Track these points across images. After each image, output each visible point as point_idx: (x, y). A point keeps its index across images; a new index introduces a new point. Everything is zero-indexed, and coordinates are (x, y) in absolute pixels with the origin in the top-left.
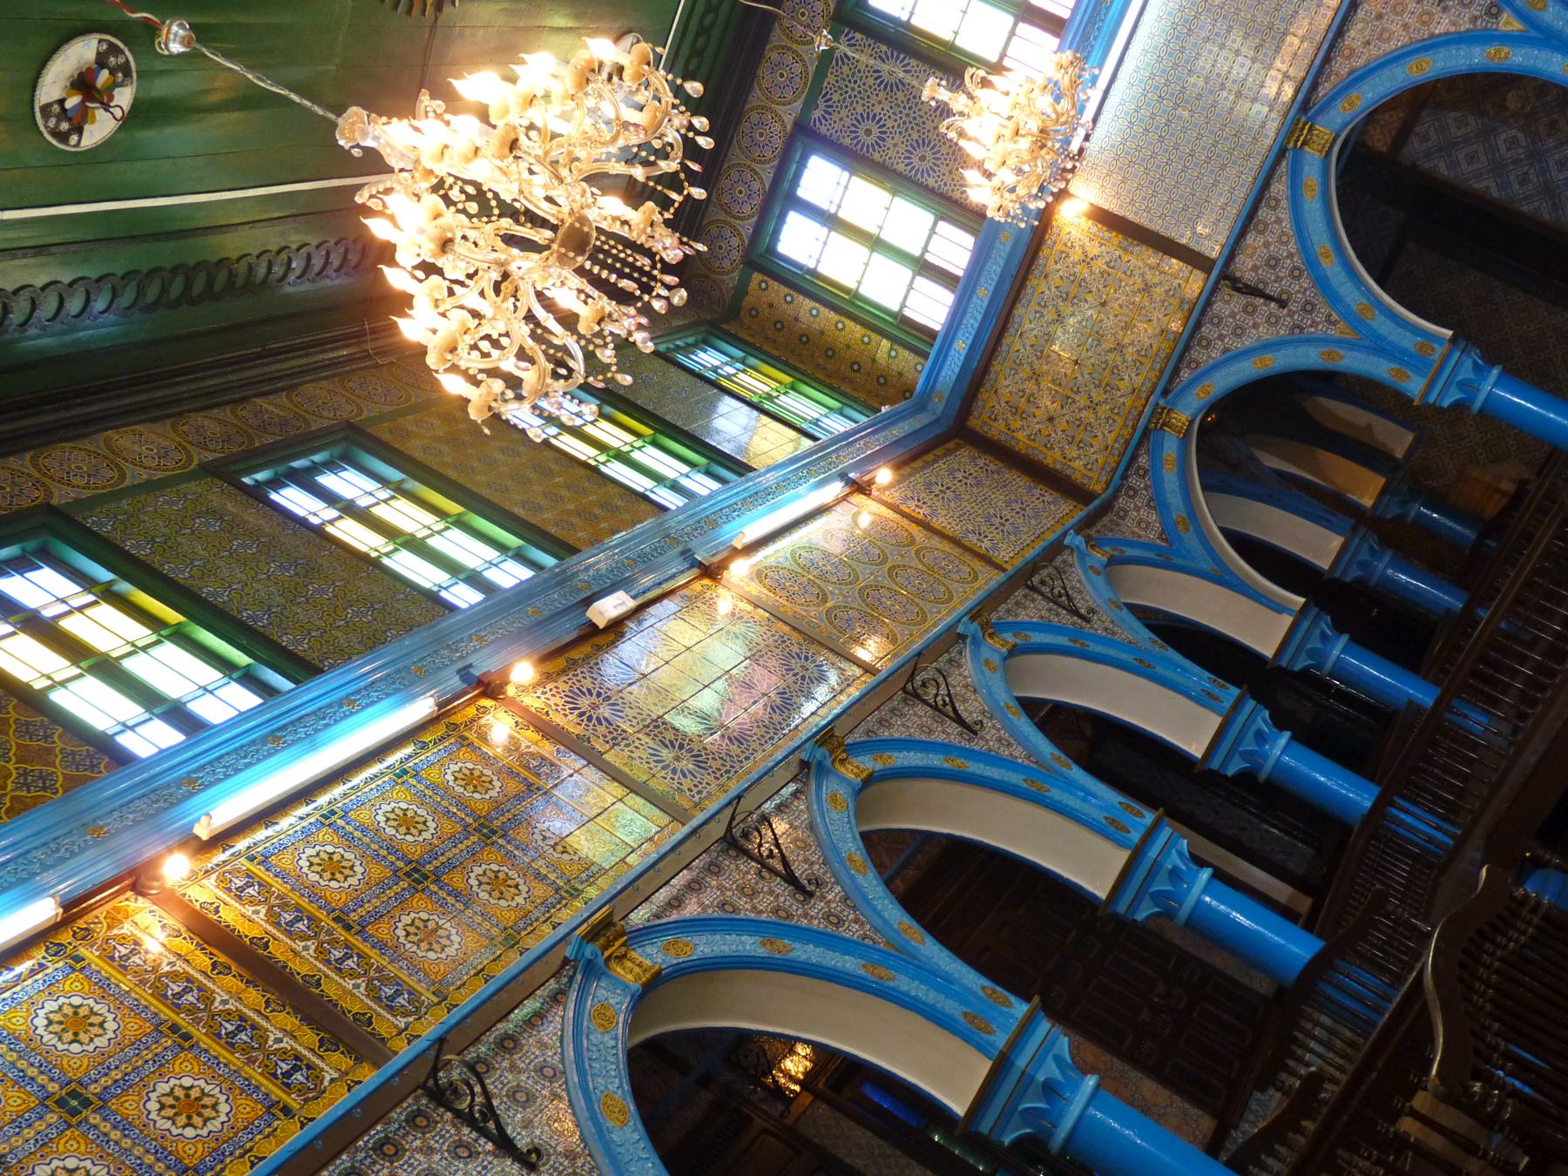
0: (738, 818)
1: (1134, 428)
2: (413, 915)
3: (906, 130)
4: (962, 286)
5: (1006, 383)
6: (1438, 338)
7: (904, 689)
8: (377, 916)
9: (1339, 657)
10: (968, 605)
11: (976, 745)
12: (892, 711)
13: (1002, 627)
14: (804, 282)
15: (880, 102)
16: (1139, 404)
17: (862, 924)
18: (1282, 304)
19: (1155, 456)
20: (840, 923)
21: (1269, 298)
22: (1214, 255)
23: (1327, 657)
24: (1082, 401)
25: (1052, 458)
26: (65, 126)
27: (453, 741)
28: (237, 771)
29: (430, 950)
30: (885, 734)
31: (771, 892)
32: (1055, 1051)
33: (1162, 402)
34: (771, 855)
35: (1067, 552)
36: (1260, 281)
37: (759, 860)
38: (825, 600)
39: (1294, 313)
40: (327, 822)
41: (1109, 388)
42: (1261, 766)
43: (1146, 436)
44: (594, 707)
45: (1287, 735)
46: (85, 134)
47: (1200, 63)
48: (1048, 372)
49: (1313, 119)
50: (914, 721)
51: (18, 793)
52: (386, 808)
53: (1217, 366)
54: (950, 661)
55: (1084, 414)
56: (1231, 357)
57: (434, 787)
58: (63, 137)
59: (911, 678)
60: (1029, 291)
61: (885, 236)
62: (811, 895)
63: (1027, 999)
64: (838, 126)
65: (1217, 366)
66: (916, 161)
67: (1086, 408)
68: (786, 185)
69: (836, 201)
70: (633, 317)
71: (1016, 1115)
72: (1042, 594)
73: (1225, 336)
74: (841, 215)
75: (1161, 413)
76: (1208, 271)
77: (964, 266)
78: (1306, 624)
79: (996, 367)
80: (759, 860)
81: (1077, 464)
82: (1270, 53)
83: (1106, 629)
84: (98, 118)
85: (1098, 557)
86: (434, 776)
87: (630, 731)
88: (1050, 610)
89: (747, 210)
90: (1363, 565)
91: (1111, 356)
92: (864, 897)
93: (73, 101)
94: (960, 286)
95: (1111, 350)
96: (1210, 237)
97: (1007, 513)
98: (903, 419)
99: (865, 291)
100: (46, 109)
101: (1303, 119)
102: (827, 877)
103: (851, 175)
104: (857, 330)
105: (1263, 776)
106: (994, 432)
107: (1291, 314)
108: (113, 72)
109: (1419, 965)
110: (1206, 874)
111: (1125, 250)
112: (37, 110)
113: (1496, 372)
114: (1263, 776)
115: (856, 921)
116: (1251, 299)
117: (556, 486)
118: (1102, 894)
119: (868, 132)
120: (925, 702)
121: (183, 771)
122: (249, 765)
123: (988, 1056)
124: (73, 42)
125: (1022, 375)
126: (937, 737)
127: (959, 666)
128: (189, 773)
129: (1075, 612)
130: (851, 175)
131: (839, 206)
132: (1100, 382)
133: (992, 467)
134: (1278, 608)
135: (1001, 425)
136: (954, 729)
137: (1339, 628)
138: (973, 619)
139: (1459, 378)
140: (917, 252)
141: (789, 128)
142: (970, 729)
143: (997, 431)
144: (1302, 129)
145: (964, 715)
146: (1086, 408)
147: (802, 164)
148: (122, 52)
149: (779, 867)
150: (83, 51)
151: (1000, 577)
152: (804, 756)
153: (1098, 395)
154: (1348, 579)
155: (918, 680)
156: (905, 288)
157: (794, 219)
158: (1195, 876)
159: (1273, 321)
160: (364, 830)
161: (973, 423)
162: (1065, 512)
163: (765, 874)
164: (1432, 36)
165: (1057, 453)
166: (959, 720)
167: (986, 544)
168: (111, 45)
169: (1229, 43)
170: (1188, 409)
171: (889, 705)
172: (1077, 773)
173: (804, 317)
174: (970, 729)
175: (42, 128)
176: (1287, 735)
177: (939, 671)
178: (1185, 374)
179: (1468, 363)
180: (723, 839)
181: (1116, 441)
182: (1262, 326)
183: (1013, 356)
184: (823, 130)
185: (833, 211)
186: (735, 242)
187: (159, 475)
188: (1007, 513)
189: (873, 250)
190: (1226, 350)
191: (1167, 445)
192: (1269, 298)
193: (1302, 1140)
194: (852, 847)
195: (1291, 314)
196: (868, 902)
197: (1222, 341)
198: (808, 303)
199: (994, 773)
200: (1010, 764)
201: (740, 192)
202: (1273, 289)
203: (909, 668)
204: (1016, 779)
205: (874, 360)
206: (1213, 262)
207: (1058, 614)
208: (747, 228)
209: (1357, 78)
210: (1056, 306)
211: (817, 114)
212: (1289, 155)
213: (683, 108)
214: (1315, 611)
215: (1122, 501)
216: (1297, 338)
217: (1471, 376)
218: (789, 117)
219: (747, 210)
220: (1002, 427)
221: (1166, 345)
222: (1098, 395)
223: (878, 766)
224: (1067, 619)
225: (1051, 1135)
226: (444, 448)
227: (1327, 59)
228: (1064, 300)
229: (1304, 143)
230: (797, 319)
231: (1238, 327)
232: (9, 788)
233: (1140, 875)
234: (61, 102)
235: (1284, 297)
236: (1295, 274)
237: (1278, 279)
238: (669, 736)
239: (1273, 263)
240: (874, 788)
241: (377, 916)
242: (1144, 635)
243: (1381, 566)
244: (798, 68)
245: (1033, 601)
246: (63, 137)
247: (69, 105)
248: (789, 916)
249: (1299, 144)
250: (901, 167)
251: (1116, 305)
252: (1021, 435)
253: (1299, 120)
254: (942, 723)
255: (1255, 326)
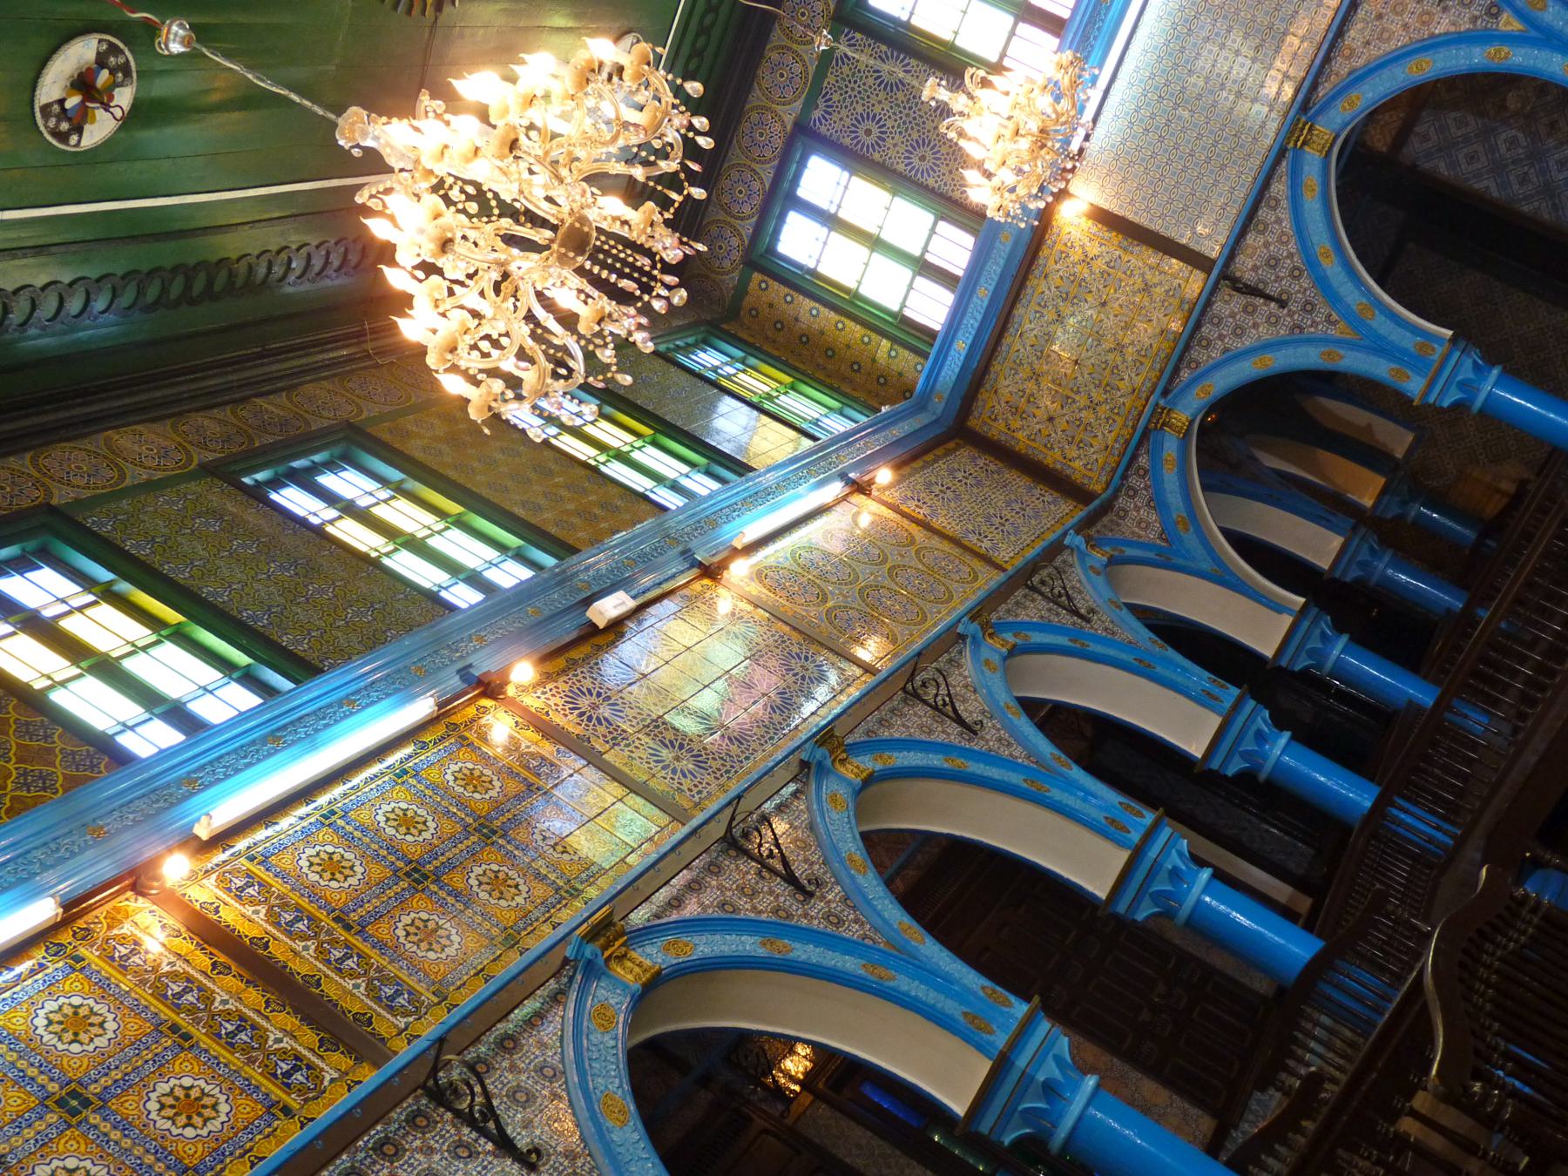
0: (738, 818)
1: (1134, 428)
2: (413, 915)
3: (906, 130)
4: (962, 286)
5: (1006, 383)
6: (1438, 338)
7: (904, 689)
8: (377, 916)
9: (1339, 657)
10: (968, 605)
11: (976, 745)
12: (892, 711)
13: (1002, 627)
14: (804, 282)
15: (880, 102)
16: (1139, 404)
17: (862, 924)
18: (1282, 304)
19: (1155, 456)
20: (840, 923)
21: (1269, 298)
22: (1214, 255)
23: (1327, 657)
24: (1082, 401)
25: (1052, 458)
26: (65, 126)
27: (453, 741)
28: (237, 771)
29: (430, 950)
30: (885, 734)
31: (771, 892)
32: (1055, 1051)
33: (1162, 402)
34: (771, 855)
35: (1067, 552)
36: (1260, 281)
37: (759, 860)
38: (825, 600)
39: (1294, 313)
40: (327, 822)
41: (1109, 388)
42: (1261, 766)
43: (1146, 436)
44: (594, 707)
45: (1287, 735)
46: (85, 134)
47: (1200, 63)
48: (1048, 372)
49: (1313, 119)
50: (914, 721)
51: (18, 793)
52: (386, 808)
53: (1217, 366)
54: (950, 661)
55: (1084, 414)
56: (1231, 357)
57: (434, 787)
58: (63, 137)
59: (911, 678)
60: (1029, 291)
61: (885, 236)
62: (811, 895)
63: (1027, 999)
64: (838, 126)
65: (1217, 366)
66: (916, 161)
67: (1086, 408)
68: (786, 185)
69: (836, 201)
70: (633, 317)
71: (1016, 1115)
72: (1042, 594)
73: (1225, 336)
74: (841, 215)
75: (1161, 413)
76: (1208, 271)
77: (964, 266)
78: (1306, 624)
79: (996, 367)
80: (759, 860)
81: (1077, 464)
82: (1270, 53)
83: (1106, 629)
84: (98, 118)
85: (1098, 557)
86: (434, 776)
87: (630, 731)
88: (1050, 610)
89: (747, 210)
90: (1363, 565)
91: (1111, 356)
92: (864, 897)
93: (73, 101)
94: (960, 286)
95: (1111, 350)
96: (1210, 237)
97: (1007, 513)
98: (903, 419)
99: (865, 291)
100: (46, 109)
101: (1303, 119)
102: (827, 877)
103: (851, 175)
104: (857, 330)
105: (1263, 776)
106: (994, 432)
107: (1291, 314)
108: (113, 72)
109: (1419, 965)
110: (1206, 874)
111: (1125, 250)
112: (37, 110)
113: (1496, 372)
114: (1263, 776)
115: (856, 921)
116: (1251, 299)
117: (556, 486)
118: (1102, 894)
119: (868, 132)
120: (925, 702)
121: (183, 771)
122: (249, 765)
123: (988, 1056)
124: (73, 42)
125: (1022, 375)
126: (937, 737)
127: (959, 666)
128: (189, 773)
129: (1075, 612)
130: (851, 175)
131: (839, 206)
132: (1100, 382)
133: (992, 467)
134: (1278, 608)
135: (1001, 425)
136: (954, 729)
137: (1339, 628)
138: (973, 619)
139: (1459, 378)
140: (917, 252)
141: (789, 128)
142: (970, 729)
143: (997, 431)
144: (1302, 129)
145: (964, 715)
146: (1086, 408)
147: (802, 164)
148: (122, 52)
149: (779, 867)
150: (83, 51)
151: (1000, 577)
152: (804, 756)
153: (1098, 395)
154: (1348, 579)
155: (918, 680)
156: (905, 288)
157: (794, 219)
158: (1195, 876)
159: (1273, 321)
160: (364, 830)
161: (973, 423)
162: (1065, 512)
163: (765, 874)
164: (1432, 36)
165: (1057, 453)
166: (959, 720)
167: (986, 544)
168: (111, 45)
169: (1229, 43)
170: (1188, 409)
171: (889, 705)
172: (1077, 773)
173: (804, 317)
174: (970, 729)
175: (42, 128)
176: (1287, 735)
177: (939, 671)
178: (1185, 374)
179: (1468, 363)
180: (723, 839)
181: (1116, 441)
182: (1262, 326)
183: (1013, 356)
184: (823, 130)
185: (833, 211)
186: (735, 242)
187: (159, 475)
188: (1007, 513)
189: (873, 250)
190: (1226, 350)
191: (1167, 445)
192: (1269, 298)
193: (1302, 1140)
194: (852, 847)
195: (1291, 314)
196: (868, 902)
197: (1222, 341)
198: (808, 303)
199: (994, 773)
200: (1010, 764)
201: (740, 192)
202: (1273, 289)
203: (909, 668)
204: (1016, 779)
205: (874, 360)
206: (1213, 262)
207: (1058, 614)
208: (747, 228)
209: (1357, 78)
210: (1056, 306)
211: (817, 114)
212: (1289, 155)
213: (683, 108)
214: (1315, 611)
215: (1122, 501)
216: (1297, 338)
217: (1471, 376)
218: (789, 117)
219: (747, 210)
220: (1002, 427)
221: (1166, 345)
222: (1098, 395)
223: (878, 766)
224: (1067, 619)
225: (1051, 1135)
226: (444, 448)
227: (1327, 59)
228: (1064, 300)
229: (1304, 143)
230: (797, 319)
231: (1238, 327)
232: (9, 788)
233: (1140, 875)
234: (61, 102)
235: (1284, 297)
236: (1295, 274)
237: (1278, 279)
238: (669, 736)
239: (1273, 263)
240: (874, 788)
241: (377, 916)
242: (1144, 635)
243: (1381, 566)
244: (798, 68)
245: (1033, 601)
246: (63, 137)
247: (69, 105)
248: (789, 916)
249: (1299, 144)
250: (901, 167)
251: (1116, 305)
252: (1021, 435)
253: (1299, 120)
254: (942, 723)
255: (1255, 326)
